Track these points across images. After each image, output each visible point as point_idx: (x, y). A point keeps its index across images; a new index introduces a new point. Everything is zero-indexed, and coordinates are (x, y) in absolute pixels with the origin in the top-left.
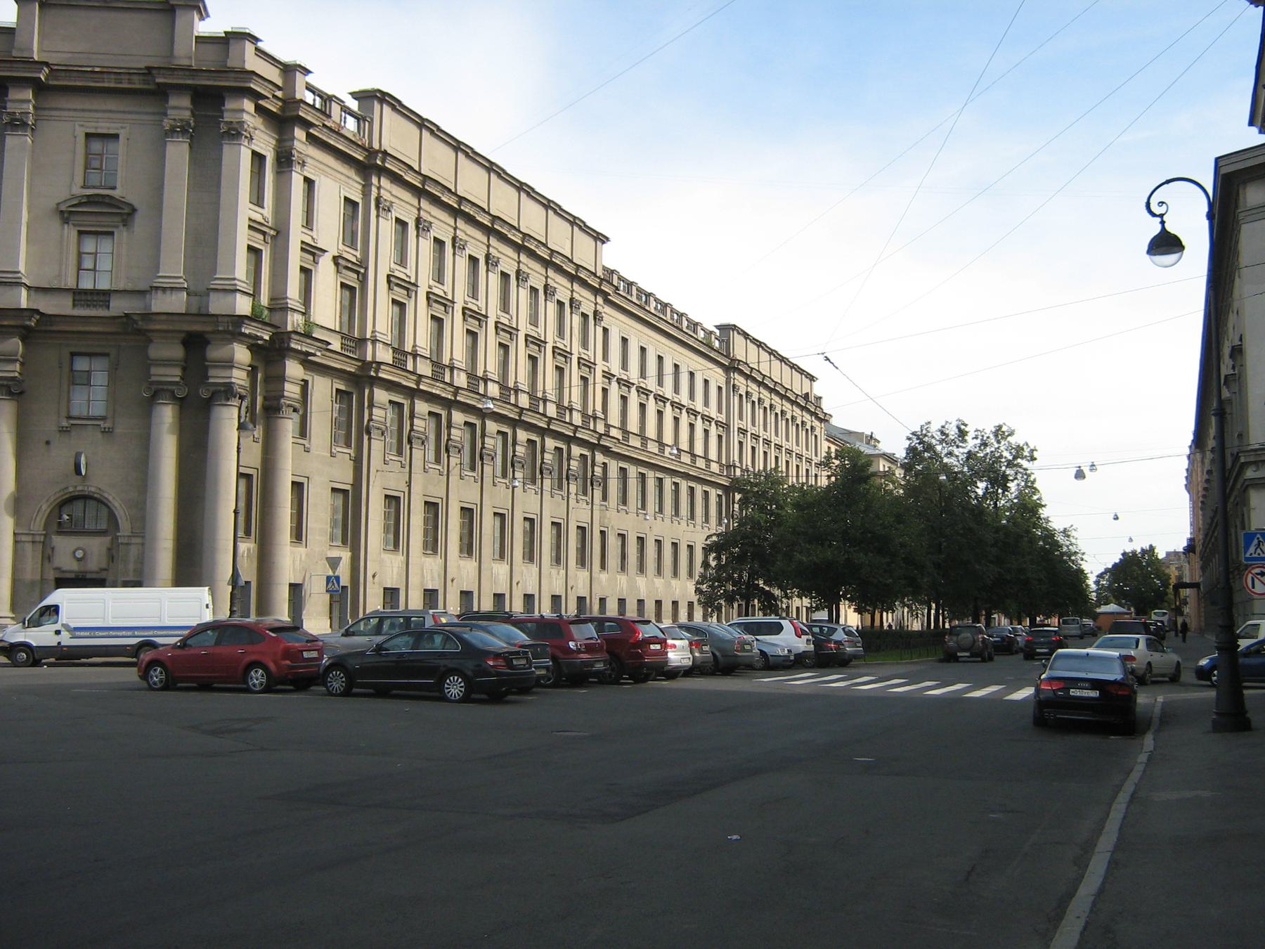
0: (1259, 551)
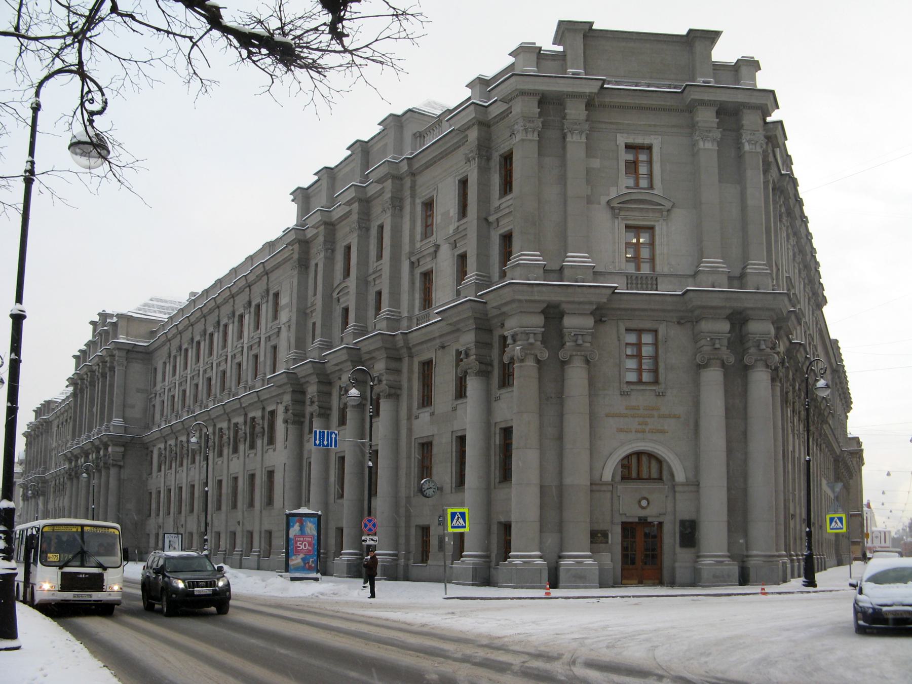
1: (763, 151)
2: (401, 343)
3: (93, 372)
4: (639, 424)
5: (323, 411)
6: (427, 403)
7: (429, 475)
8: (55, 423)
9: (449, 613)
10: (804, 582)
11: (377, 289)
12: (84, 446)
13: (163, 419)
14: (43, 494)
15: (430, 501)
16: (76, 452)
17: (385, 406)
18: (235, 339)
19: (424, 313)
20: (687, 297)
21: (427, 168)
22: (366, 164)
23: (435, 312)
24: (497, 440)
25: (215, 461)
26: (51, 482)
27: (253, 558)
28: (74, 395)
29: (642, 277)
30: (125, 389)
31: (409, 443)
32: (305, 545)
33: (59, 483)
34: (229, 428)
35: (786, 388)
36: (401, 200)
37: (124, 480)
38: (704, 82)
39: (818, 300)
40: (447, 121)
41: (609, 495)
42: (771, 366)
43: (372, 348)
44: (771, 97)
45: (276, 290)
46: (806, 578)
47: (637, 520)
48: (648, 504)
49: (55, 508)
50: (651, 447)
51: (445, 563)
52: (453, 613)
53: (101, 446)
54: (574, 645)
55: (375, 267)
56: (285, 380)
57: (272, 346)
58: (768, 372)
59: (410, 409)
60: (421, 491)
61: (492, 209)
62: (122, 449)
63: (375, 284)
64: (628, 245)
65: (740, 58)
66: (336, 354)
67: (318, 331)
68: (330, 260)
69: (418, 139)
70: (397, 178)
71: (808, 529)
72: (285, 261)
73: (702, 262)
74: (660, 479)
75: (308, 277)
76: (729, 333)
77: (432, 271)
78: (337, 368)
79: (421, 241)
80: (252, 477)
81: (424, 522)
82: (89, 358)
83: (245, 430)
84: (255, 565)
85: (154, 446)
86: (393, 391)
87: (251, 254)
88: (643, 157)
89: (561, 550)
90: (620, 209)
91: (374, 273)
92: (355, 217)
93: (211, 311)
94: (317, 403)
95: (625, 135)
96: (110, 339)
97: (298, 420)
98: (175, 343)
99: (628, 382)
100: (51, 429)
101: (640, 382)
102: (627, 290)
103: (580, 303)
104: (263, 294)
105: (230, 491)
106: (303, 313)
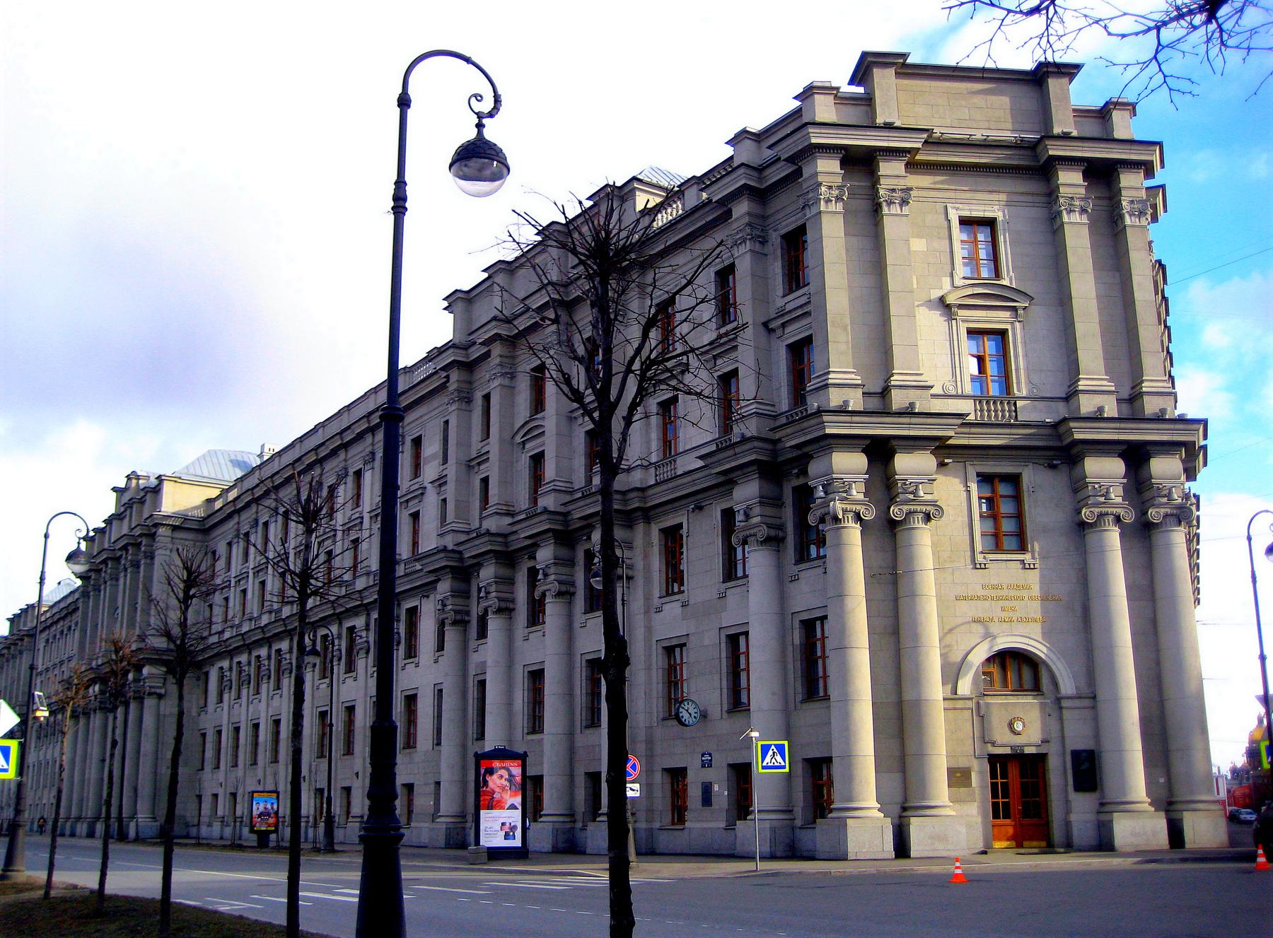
0: (773, 760)
17: (494, 624)
24: (797, 637)
31: (648, 648)
37: (164, 715)
47: (1008, 751)
59: (648, 598)
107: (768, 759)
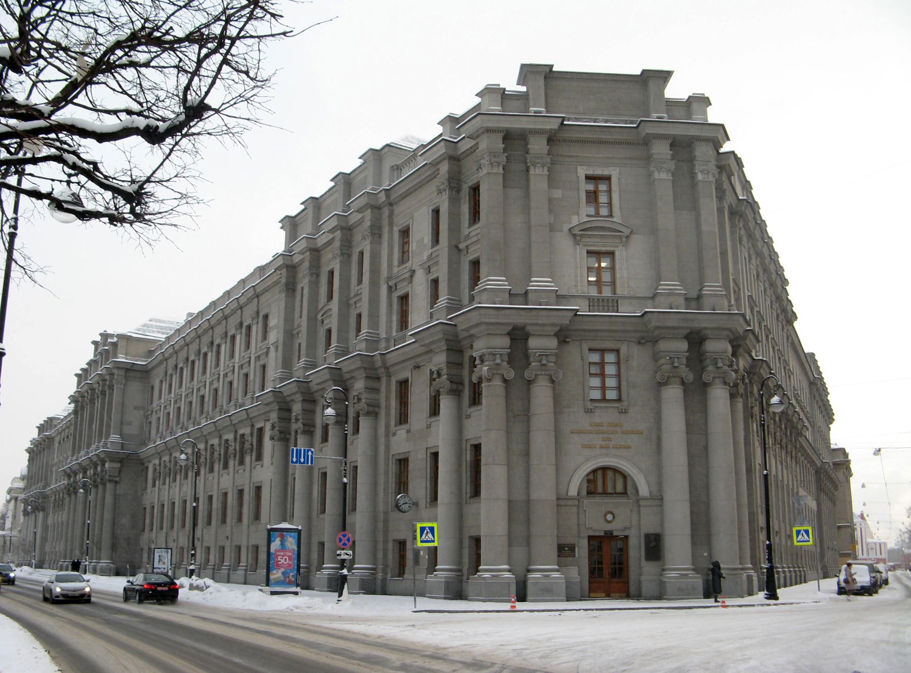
1: (716, 180)
2: (379, 364)
3: (93, 390)
4: (603, 440)
5: (307, 428)
6: (404, 421)
7: (406, 491)
8: (57, 439)
9: (410, 626)
10: (766, 594)
11: (358, 312)
12: (82, 463)
13: (159, 435)
14: (43, 509)
15: (406, 516)
16: (76, 468)
17: (364, 423)
18: (227, 358)
19: (401, 334)
20: (646, 318)
21: (403, 198)
22: (348, 194)
23: (409, 334)
24: (468, 456)
25: (207, 477)
26: (51, 497)
27: (240, 573)
28: (75, 412)
29: (608, 300)
30: (123, 406)
31: (387, 459)
32: (286, 559)
33: (59, 498)
34: (220, 445)
35: (751, 403)
36: (380, 228)
37: (119, 495)
38: (658, 118)
39: (787, 316)
40: (420, 156)
41: (575, 509)
42: (729, 383)
43: (353, 367)
44: (722, 131)
45: (266, 312)
46: (767, 591)
47: (603, 534)
48: (614, 518)
49: (54, 524)
50: (595, 464)
51: (414, 577)
52: (414, 625)
53: (99, 462)
54: (511, 655)
55: (356, 290)
56: (272, 399)
57: (229, 382)
58: (727, 389)
60: (397, 507)
61: (462, 237)
62: (119, 465)
63: (356, 307)
64: (590, 269)
65: (691, 95)
66: (318, 375)
67: (303, 352)
68: (314, 285)
69: (396, 172)
70: (376, 208)
71: (768, 542)
72: (276, 283)
73: (660, 285)
74: (625, 493)
75: (295, 300)
76: (687, 352)
77: (408, 294)
78: (320, 387)
79: (399, 266)
80: (241, 492)
81: (401, 537)
82: (90, 376)
83: (235, 447)
84: (242, 579)
85: (150, 462)
86: (371, 409)
87: (243, 278)
88: (603, 187)
89: (529, 564)
90: (582, 236)
91: (356, 295)
92: (337, 244)
93: (206, 331)
94: (301, 421)
95: (585, 167)
96: (110, 358)
97: (284, 437)
98: (171, 362)
99: (591, 400)
100: (53, 445)
101: (604, 399)
102: (589, 312)
103: (544, 325)
104: (254, 316)
105: (220, 506)
106: (290, 334)
107: (423, 536)
